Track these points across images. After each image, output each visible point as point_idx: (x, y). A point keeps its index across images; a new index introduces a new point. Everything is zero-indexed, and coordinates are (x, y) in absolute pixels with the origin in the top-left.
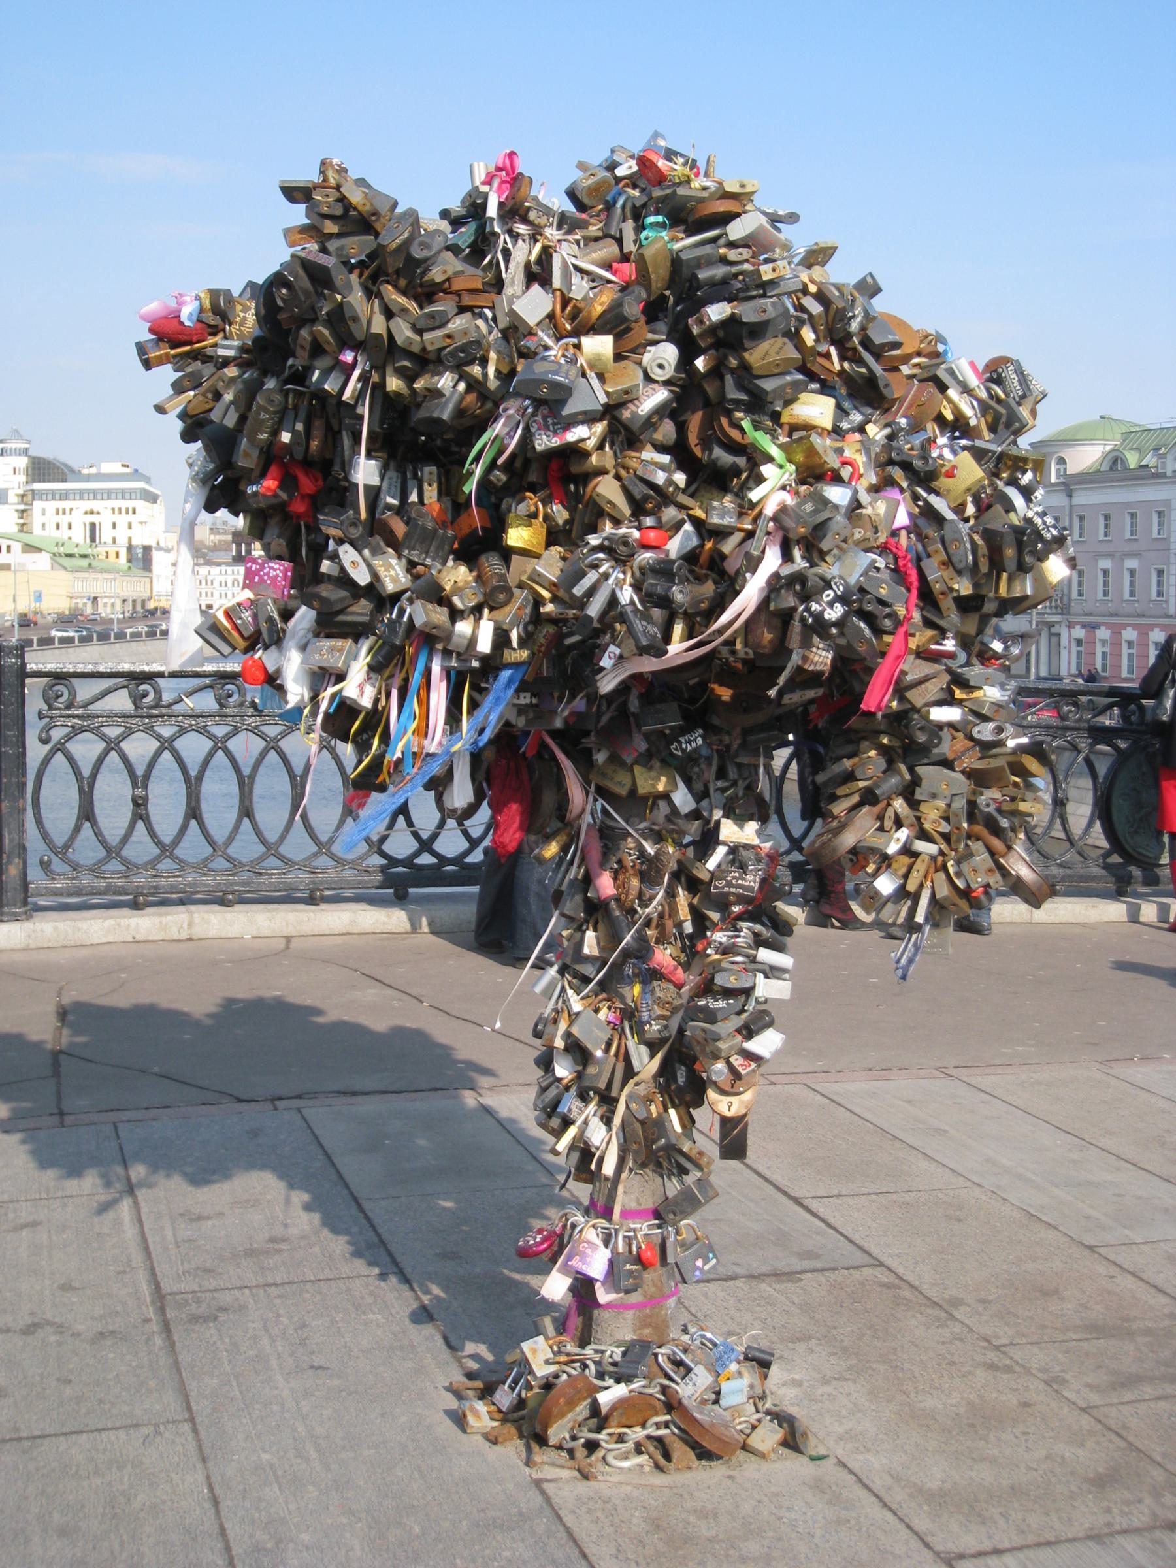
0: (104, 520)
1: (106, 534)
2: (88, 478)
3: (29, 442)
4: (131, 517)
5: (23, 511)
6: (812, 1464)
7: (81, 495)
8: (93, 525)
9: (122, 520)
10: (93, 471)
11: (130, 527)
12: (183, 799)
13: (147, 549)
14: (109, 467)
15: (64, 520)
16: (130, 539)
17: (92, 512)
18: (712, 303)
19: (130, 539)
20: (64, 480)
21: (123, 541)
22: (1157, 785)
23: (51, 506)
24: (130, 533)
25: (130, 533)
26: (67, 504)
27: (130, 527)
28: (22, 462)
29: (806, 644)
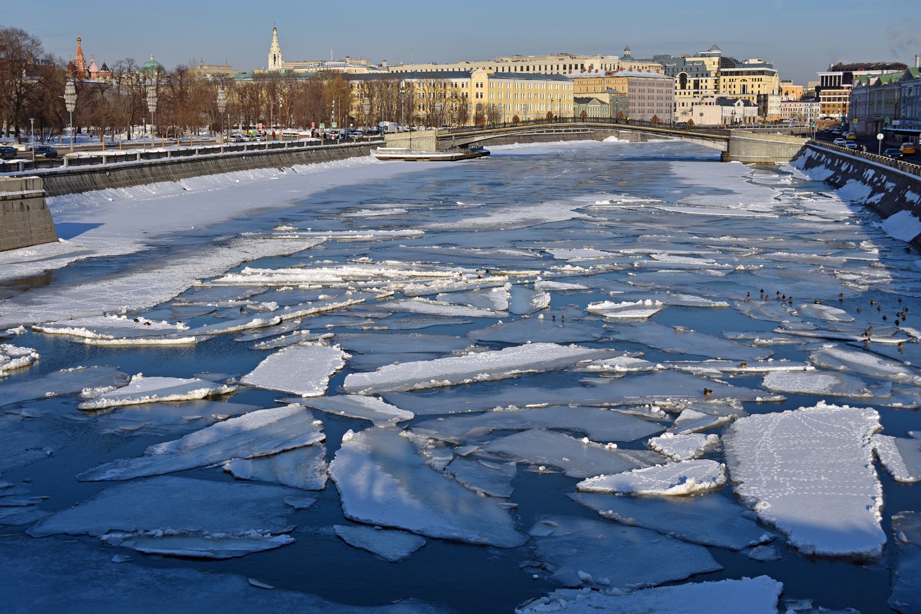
0: (749, 83)
1: (749, 90)
2: (745, 66)
3: (916, 56)
4: (760, 83)
5: (716, 80)
6: (676, 464)
7: (737, 73)
8: (744, 86)
9: (756, 84)
10: (746, 63)
11: (759, 87)
12: (265, 480)
13: (766, 96)
14: (752, 61)
15: (733, 83)
16: (759, 91)
17: (744, 80)
18: (747, 576)
19: (759, 91)
20: (734, 67)
21: (756, 91)
22: (892, 547)
23: (727, 78)
24: (759, 89)
25: (759, 89)
26: (734, 77)
27: (759, 87)
28: (716, 59)
29: (702, 443)
